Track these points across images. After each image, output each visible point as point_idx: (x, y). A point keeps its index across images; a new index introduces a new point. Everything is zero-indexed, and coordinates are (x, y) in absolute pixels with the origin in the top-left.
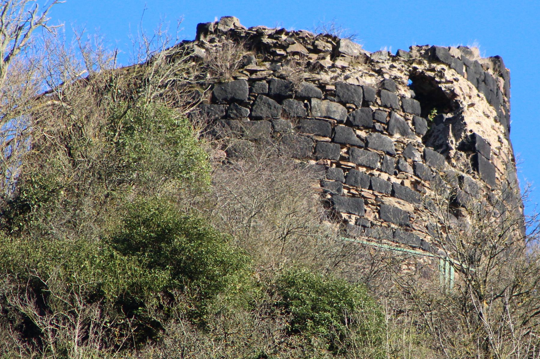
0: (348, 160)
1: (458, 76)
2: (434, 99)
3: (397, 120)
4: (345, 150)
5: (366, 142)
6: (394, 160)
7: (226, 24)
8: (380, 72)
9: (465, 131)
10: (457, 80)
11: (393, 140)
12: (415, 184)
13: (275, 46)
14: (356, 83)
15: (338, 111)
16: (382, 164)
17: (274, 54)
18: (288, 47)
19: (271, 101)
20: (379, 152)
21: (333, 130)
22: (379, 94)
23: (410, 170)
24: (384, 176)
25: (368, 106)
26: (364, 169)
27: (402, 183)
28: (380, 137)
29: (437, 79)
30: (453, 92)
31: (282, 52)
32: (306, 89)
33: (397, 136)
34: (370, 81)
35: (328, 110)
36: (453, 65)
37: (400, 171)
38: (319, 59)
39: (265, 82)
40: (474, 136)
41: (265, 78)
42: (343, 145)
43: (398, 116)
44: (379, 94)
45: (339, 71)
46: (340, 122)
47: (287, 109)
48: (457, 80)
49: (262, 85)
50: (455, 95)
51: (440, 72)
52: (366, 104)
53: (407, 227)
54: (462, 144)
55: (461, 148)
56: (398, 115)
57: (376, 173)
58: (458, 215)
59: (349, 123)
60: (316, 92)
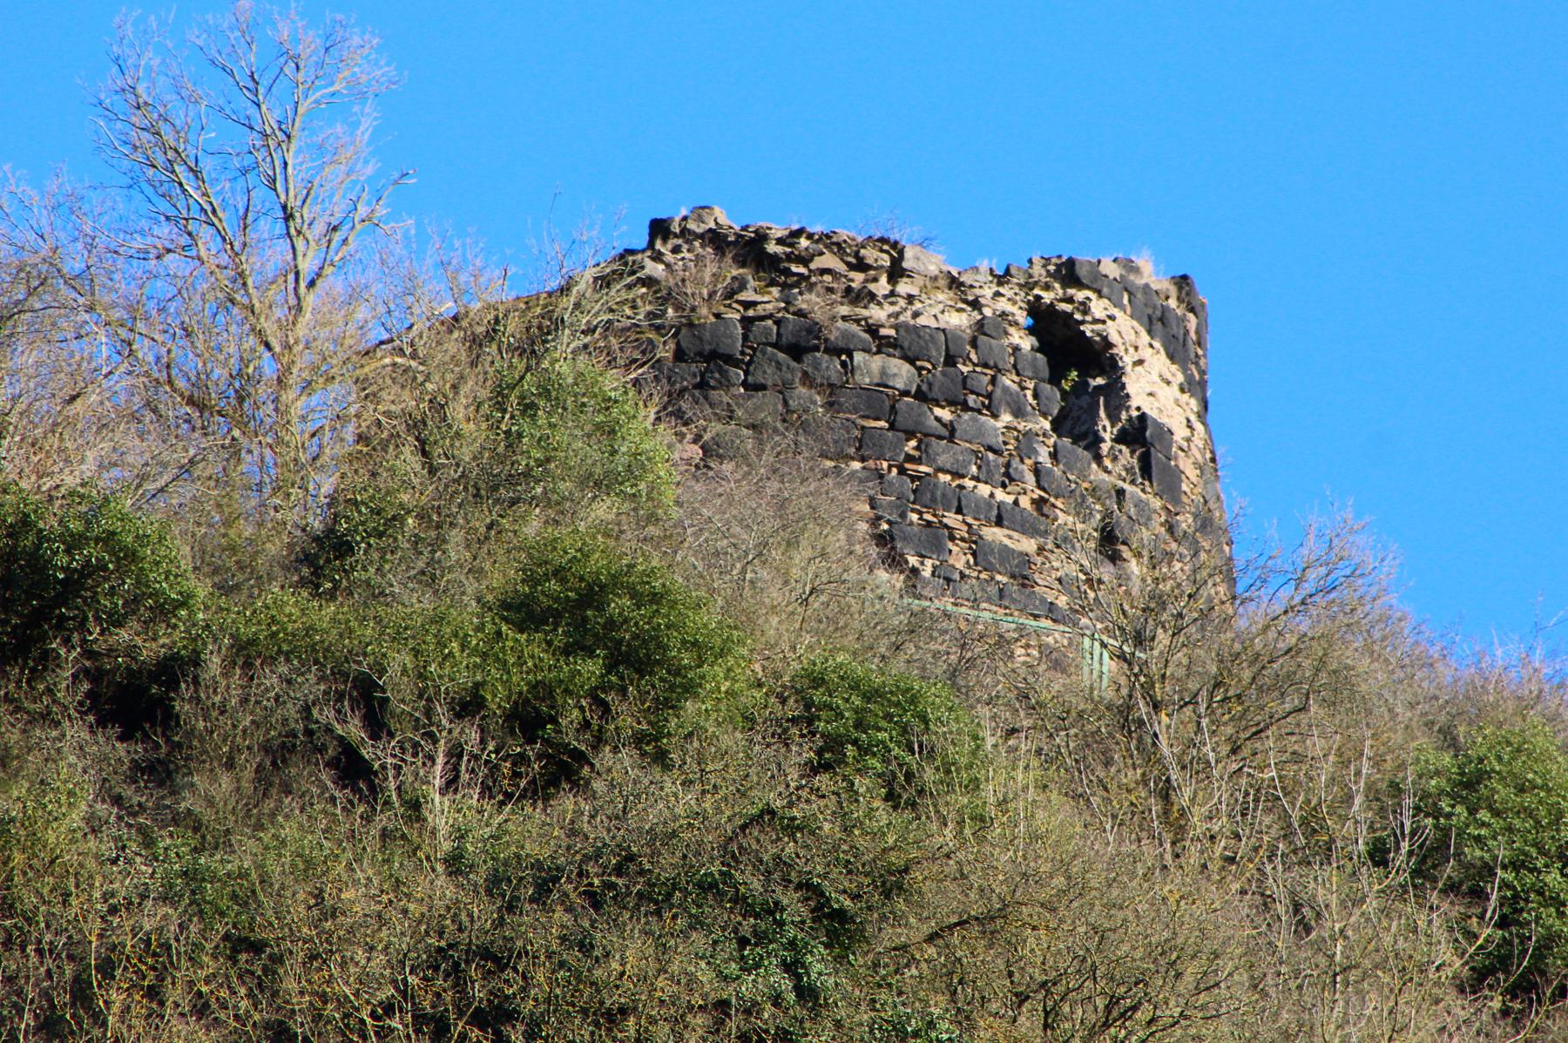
0: (918, 461)
3: (1006, 389)
4: (913, 443)
6: (1001, 460)
7: (701, 220)
8: (976, 305)
10: (1112, 318)
12: (1039, 503)
13: (790, 258)
14: (934, 324)
15: (902, 373)
16: (979, 468)
17: (788, 273)
18: (811, 260)
19: (781, 356)
20: (974, 447)
21: (893, 407)
23: (1030, 478)
24: (984, 490)
25: (954, 365)
26: (948, 477)
27: (1016, 503)
28: (974, 420)
29: (1078, 316)
31: (802, 270)
32: (846, 335)
33: (1007, 418)
34: (959, 321)
35: (883, 372)
36: (1105, 291)
37: (1012, 480)
39: (770, 322)
40: (1143, 417)
41: (770, 316)
42: (910, 435)
43: (1008, 382)
45: (902, 303)
46: (906, 393)
47: (810, 370)
48: (1112, 318)
51: (1083, 304)
52: (950, 361)
53: (1025, 581)
54: (1123, 431)
55: (1121, 438)
56: (1008, 381)
57: (969, 483)
58: (1115, 558)
59: (920, 396)
60: (862, 340)
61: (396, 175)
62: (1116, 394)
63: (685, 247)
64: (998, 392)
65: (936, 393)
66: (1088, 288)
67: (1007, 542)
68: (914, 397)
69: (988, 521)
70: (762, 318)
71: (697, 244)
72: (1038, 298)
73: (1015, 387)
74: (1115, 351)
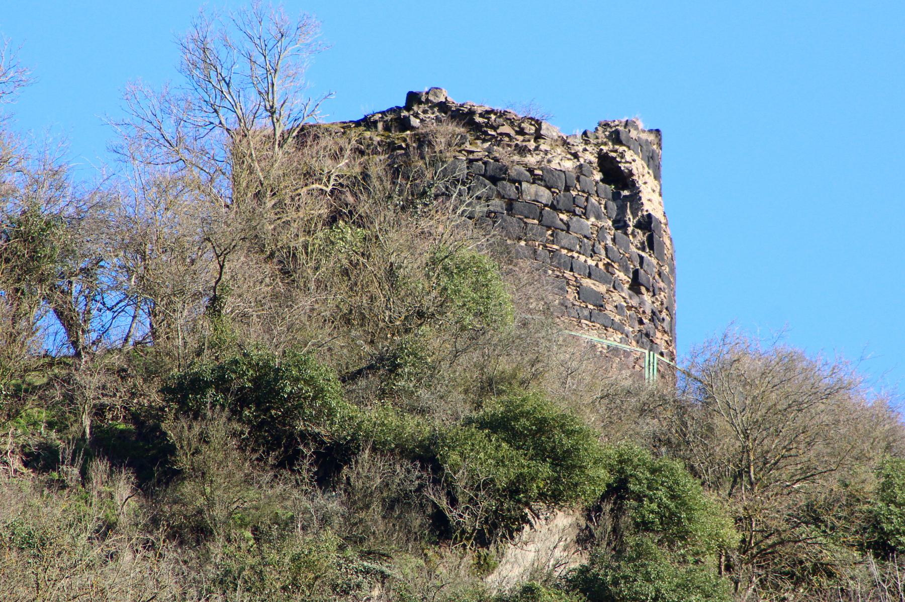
0: (553, 242)
1: (635, 157)
2: (616, 176)
3: (593, 204)
4: (550, 232)
5: (567, 225)
6: (591, 243)
7: (436, 95)
8: (576, 156)
9: (642, 210)
10: (634, 161)
11: (589, 223)
12: (607, 265)
13: (487, 125)
14: (559, 168)
15: (545, 195)
16: (580, 247)
17: (486, 133)
18: (498, 128)
19: (487, 181)
20: (579, 236)
21: (541, 213)
22: (578, 180)
23: (603, 252)
24: (582, 258)
25: (569, 191)
26: (566, 251)
27: (597, 265)
28: (579, 221)
29: (618, 159)
30: (630, 171)
31: (493, 133)
32: (520, 174)
33: (593, 219)
34: (569, 165)
35: (536, 194)
36: (632, 146)
37: (595, 253)
38: (524, 141)
39: (480, 163)
40: (649, 216)
41: (481, 159)
42: (549, 228)
43: (594, 201)
44: (578, 179)
45: (542, 154)
46: (546, 205)
47: (501, 190)
48: (634, 161)
49: (479, 166)
50: (631, 174)
51: (622, 153)
52: (567, 189)
53: (601, 307)
54: (639, 222)
55: (638, 225)
56: (594, 200)
57: (576, 255)
58: (639, 293)
59: (553, 207)
60: (526, 176)
61: (326, 93)
62: (635, 199)
63: (430, 112)
64: (589, 205)
65: (560, 206)
66: (625, 145)
67: (593, 287)
68: (550, 207)
69: (584, 275)
70: (477, 160)
71: (436, 109)
72: (602, 150)
73: (597, 203)
74: (634, 178)
